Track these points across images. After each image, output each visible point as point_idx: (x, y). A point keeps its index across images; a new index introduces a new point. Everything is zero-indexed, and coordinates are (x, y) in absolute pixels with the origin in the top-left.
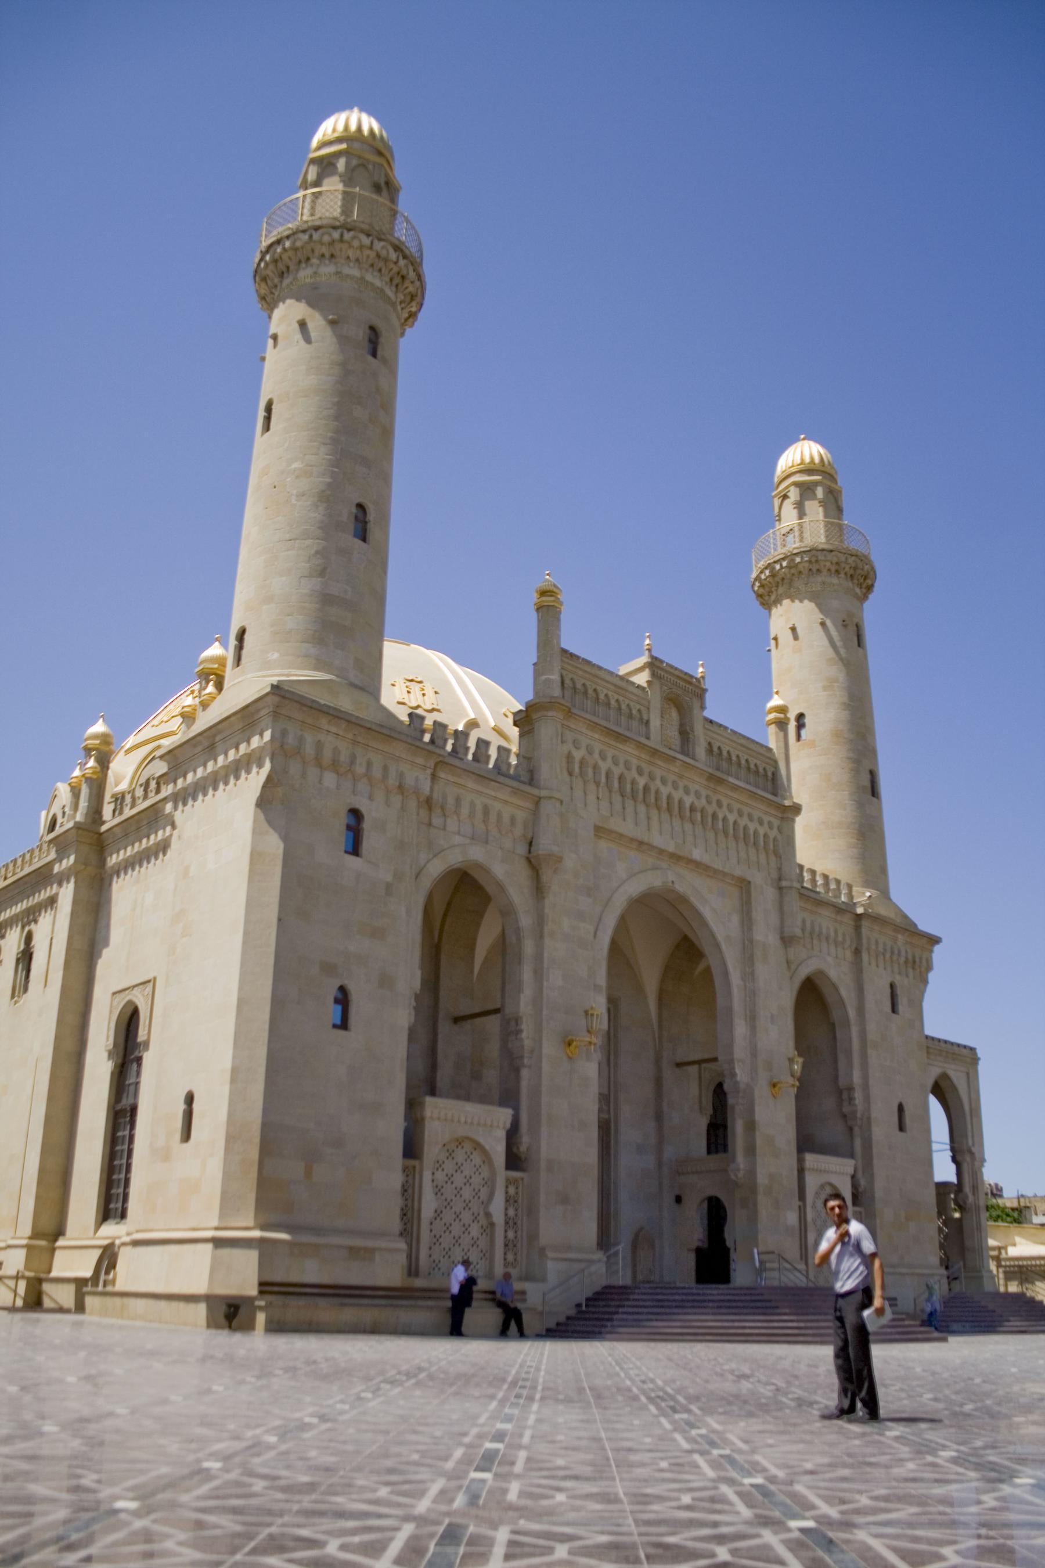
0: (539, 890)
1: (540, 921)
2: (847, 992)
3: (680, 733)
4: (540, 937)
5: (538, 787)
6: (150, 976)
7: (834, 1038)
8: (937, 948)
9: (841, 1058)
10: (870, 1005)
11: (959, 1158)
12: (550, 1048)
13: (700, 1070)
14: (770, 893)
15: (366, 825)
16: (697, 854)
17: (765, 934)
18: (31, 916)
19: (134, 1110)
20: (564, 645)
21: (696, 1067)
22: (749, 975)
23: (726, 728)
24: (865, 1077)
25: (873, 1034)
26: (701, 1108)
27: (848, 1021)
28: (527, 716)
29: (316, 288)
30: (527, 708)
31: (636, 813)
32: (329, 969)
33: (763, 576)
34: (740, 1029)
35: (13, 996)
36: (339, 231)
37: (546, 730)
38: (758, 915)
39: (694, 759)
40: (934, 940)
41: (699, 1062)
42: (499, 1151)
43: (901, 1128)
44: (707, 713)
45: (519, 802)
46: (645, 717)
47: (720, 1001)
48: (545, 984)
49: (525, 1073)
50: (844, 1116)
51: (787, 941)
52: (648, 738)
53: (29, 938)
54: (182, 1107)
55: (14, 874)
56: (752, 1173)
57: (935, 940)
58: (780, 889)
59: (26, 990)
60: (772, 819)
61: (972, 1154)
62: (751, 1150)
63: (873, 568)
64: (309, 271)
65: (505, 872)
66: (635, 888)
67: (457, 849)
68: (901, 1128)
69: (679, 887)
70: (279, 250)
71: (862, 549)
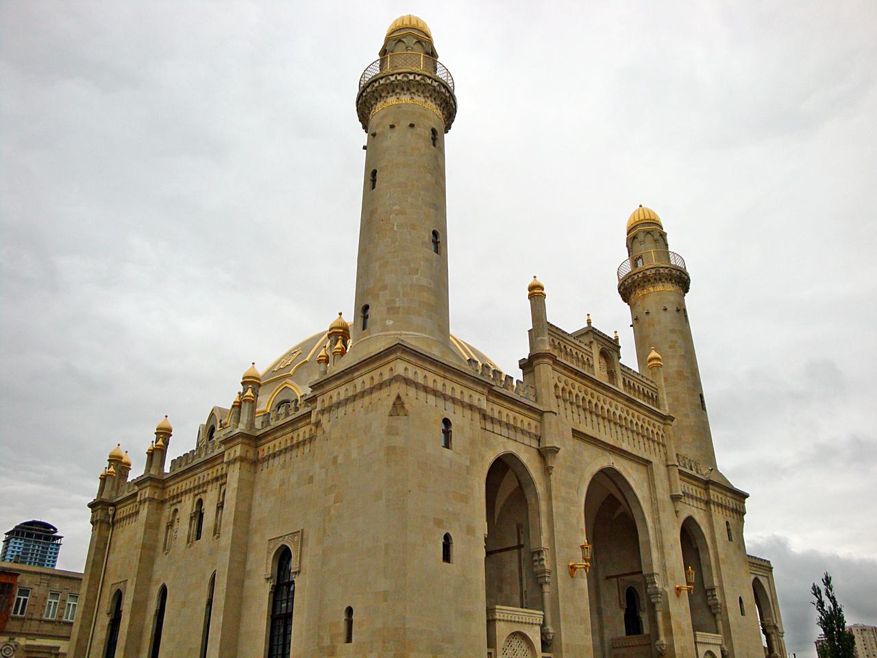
0: (547, 471)
1: (549, 490)
2: (705, 529)
3: (608, 373)
4: (550, 498)
5: (542, 404)
6: (299, 529)
7: (699, 559)
8: (747, 500)
9: (704, 569)
10: (718, 536)
11: (768, 631)
12: (561, 571)
13: (618, 580)
14: (662, 469)
15: (453, 429)
16: (625, 446)
17: (663, 495)
18: (202, 487)
19: (289, 616)
20: (548, 321)
21: (615, 579)
22: (657, 520)
23: (631, 369)
24: (721, 581)
25: (721, 556)
26: (620, 604)
27: (707, 546)
28: (529, 362)
29: (399, 107)
30: (529, 358)
31: (592, 421)
32: (438, 523)
33: (626, 283)
34: (655, 555)
35: (188, 542)
36: (413, 75)
37: (546, 371)
38: (658, 483)
39: (617, 387)
40: (745, 496)
41: (617, 576)
42: (537, 640)
43: (743, 614)
44: (621, 361)
45: (533, 415)
46: (591, 363)
47: (641, 538)
48: (555, 529)
49: (546, 588)
50: (709, 607)
51: (675, 499)
52: (594, 375)
53: (200, 502)
54: (344, 617)
55: (186, 464)
56: (672, 646)
57: (746, 496)
58: (667, 466)
59: (198, 537)
60: (659, 424)
61: (775, 627)
62: (669, 632)
63: (689, 278)
64: (394, 98)
65: (528, 458)
66: (595, 468)
67: (502, 445)
68: (743, 614)
69: (617, 467)
70: (376, 85)
71: (680, 264)
